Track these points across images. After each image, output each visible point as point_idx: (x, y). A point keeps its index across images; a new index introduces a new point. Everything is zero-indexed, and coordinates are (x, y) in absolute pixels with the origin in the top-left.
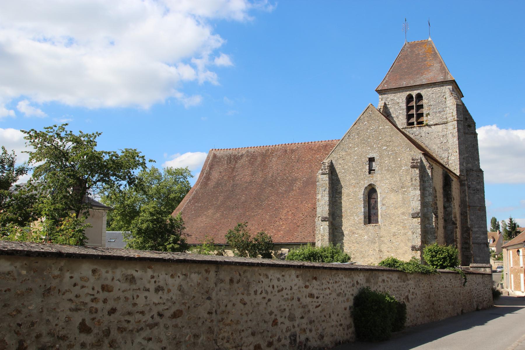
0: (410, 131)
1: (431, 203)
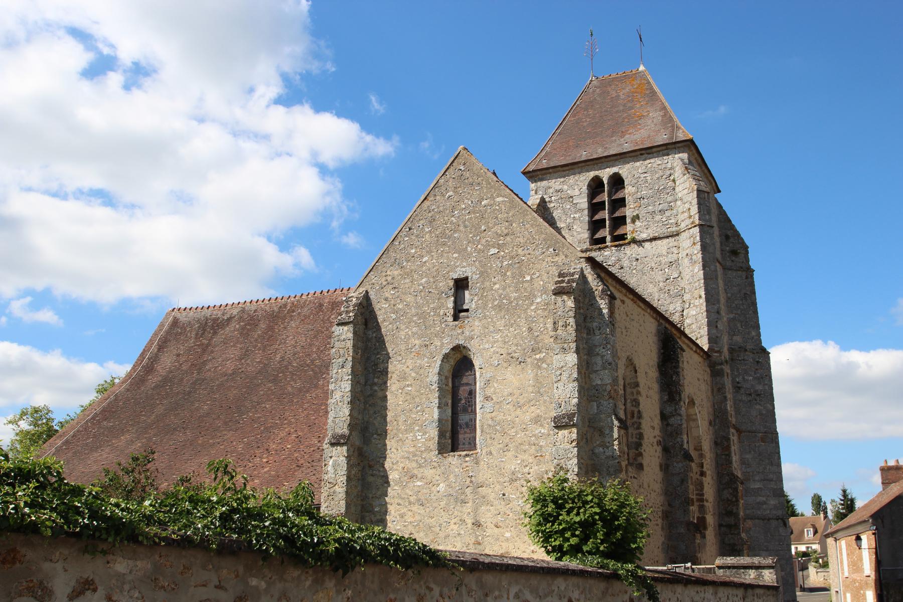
1: (609, 388)
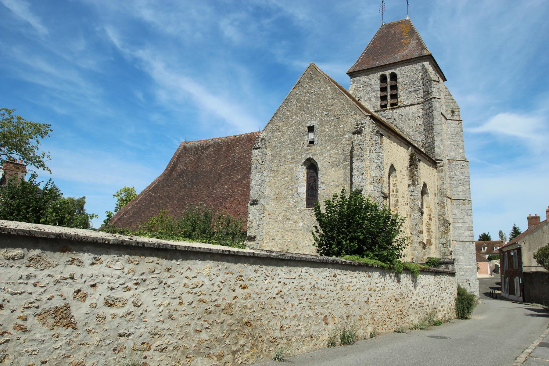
0: (381, 116)
